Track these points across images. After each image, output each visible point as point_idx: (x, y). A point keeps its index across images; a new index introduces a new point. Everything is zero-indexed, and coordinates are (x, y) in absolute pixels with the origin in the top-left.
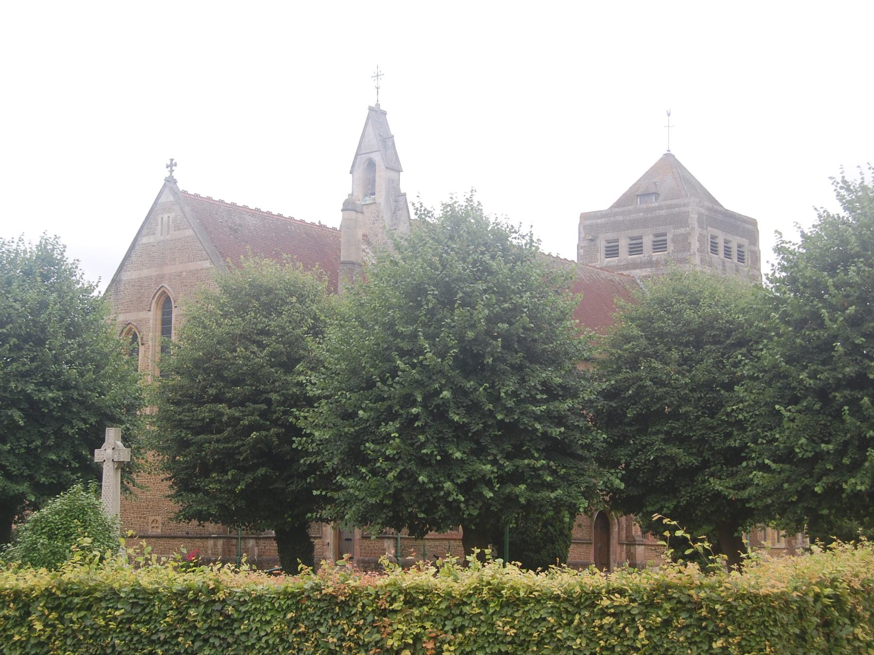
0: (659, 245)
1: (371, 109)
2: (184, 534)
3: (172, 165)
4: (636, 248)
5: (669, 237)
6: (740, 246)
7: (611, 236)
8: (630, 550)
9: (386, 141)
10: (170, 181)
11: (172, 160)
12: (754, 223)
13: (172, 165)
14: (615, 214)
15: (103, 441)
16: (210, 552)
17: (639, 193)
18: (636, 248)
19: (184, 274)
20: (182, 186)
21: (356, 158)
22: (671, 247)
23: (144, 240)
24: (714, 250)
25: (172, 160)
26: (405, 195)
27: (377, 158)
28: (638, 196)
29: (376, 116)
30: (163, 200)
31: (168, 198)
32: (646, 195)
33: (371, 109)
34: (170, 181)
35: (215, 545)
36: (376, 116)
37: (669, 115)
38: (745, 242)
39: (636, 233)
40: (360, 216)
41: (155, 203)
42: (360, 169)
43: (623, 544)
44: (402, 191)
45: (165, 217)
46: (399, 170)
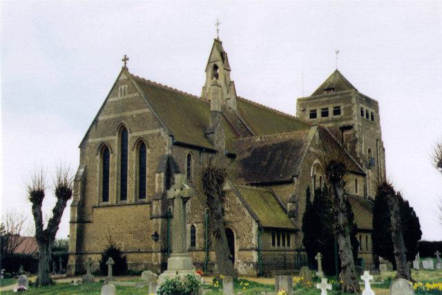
0: (337, 112)
1: (215, 40)
2: (137, 250)
3: (125, 59)
4: (325, 114)
5: (342, 108)
6: (372, 113)
7: (312, 108)
8: (422, 263)
9: (223, 56)
10: (125, 69)
11: (125, 56)
12: (377, 103)
13: (125, 59)
14: (315, 99)
15: (49, 221)
16: (153, 260)
17: (326, 87)
18: (325, 114)
19: (134, 116)
20: (131, 71)
21: (208, 65)
22: (342, 113)
23: (111, 99)
24: (362, 115)
25: (125, 56)
26: (233, 82)
27: (218, 62)
28: (324, 90)
29: (218, 43)
30: (122, 78)
31: (124, 77)
32: (329, 89)
33: (215, 40)
34: (125, 69)
35: (157, 256)
36: (218, 43)
37: (337, 52)
38: (374, 111)
39: (325, 107)
40: (219, 88)
41: (117, 80)
42: (211, 70)
43: (75, 223)
44: (232, 80)
45: (123, 87)
46: (229, 71)
